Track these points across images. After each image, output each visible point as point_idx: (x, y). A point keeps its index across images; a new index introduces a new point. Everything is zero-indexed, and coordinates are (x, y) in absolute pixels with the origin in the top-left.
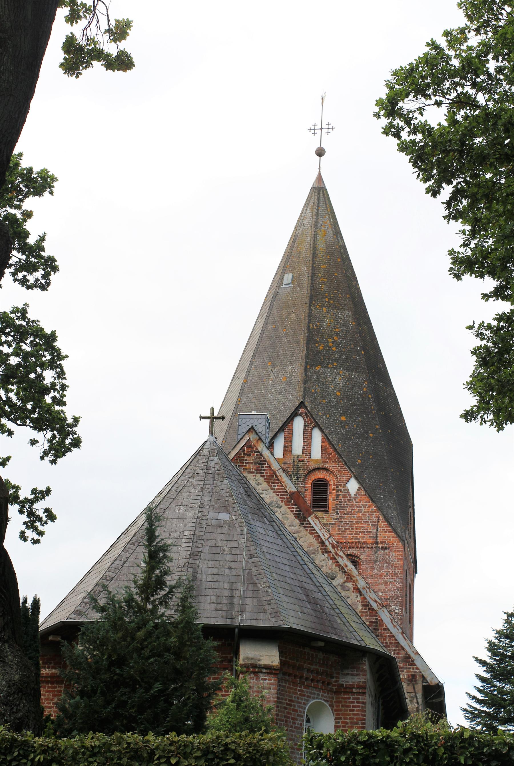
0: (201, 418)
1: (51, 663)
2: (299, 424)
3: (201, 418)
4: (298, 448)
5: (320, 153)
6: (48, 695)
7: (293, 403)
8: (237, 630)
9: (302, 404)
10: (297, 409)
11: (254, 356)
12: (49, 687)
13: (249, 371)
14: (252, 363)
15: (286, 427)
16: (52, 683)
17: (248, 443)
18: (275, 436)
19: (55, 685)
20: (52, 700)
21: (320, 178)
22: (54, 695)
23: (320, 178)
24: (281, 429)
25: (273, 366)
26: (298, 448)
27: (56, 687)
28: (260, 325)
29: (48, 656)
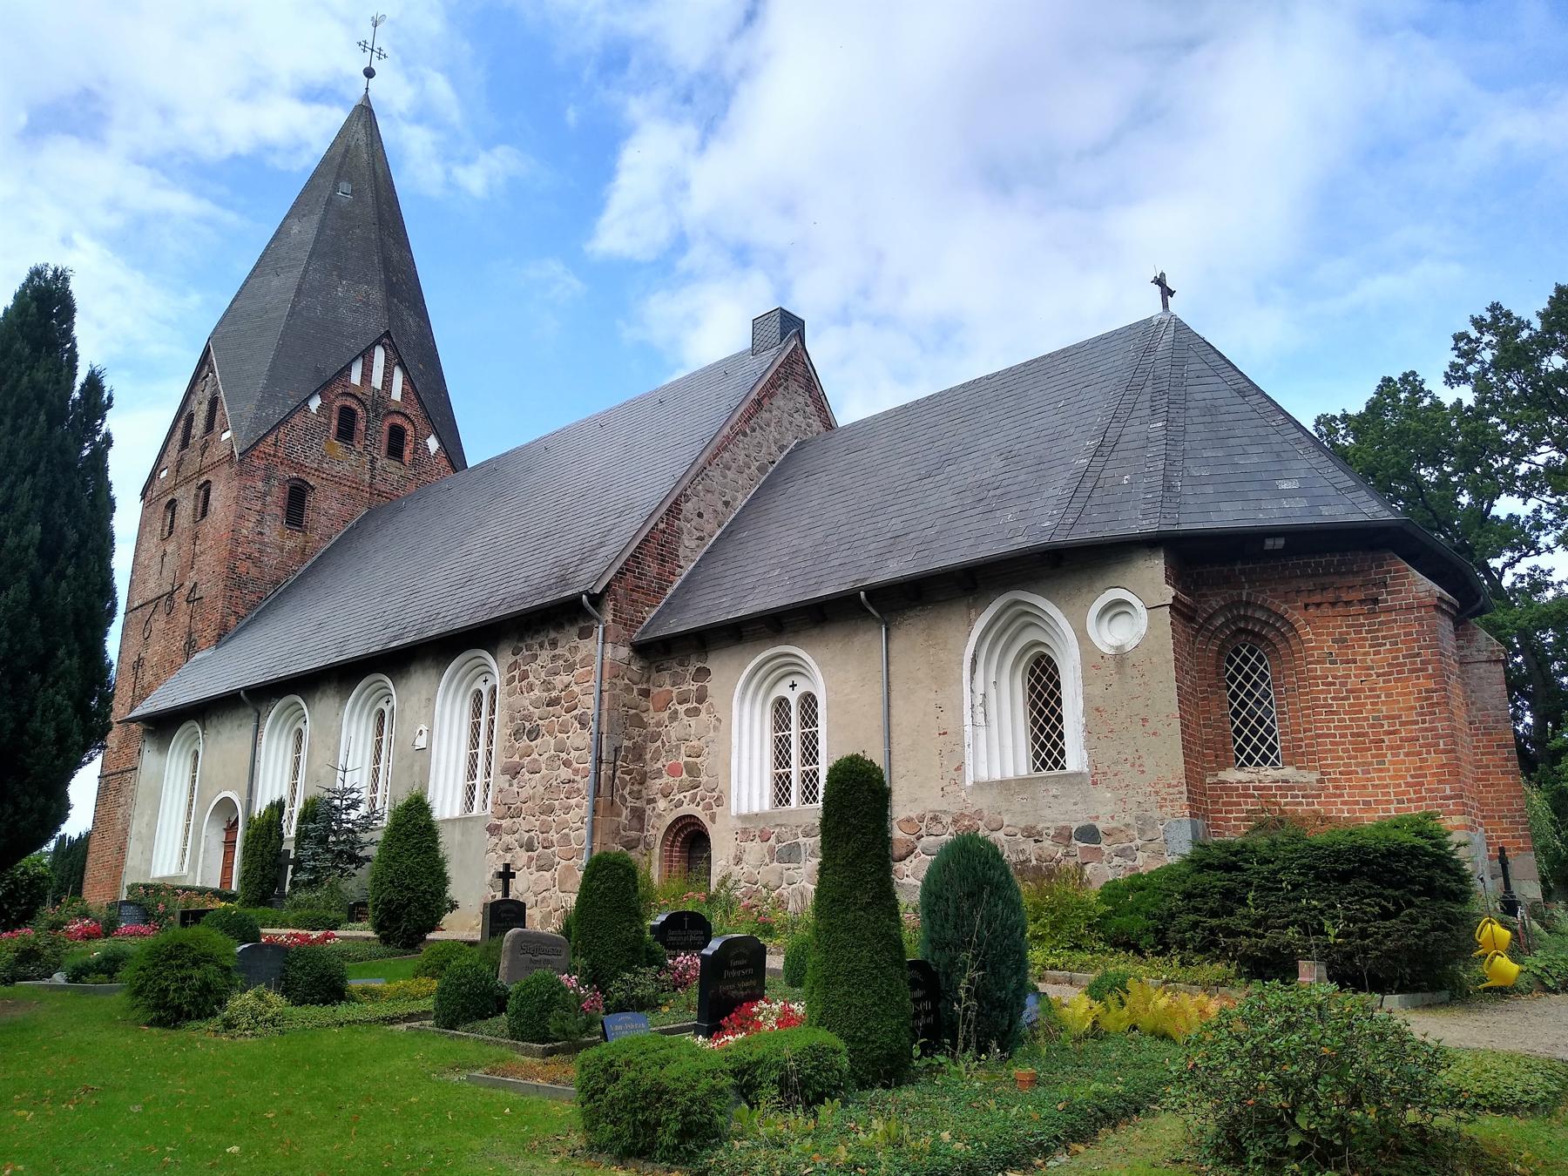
2: (379, 355)
4: (377, 380)
7: (376, 324)
13: (306, 271)
15: (366, 355)
21: (366, 97)
23: (366, 97)
25: (341, 277)
26: (377, 380)
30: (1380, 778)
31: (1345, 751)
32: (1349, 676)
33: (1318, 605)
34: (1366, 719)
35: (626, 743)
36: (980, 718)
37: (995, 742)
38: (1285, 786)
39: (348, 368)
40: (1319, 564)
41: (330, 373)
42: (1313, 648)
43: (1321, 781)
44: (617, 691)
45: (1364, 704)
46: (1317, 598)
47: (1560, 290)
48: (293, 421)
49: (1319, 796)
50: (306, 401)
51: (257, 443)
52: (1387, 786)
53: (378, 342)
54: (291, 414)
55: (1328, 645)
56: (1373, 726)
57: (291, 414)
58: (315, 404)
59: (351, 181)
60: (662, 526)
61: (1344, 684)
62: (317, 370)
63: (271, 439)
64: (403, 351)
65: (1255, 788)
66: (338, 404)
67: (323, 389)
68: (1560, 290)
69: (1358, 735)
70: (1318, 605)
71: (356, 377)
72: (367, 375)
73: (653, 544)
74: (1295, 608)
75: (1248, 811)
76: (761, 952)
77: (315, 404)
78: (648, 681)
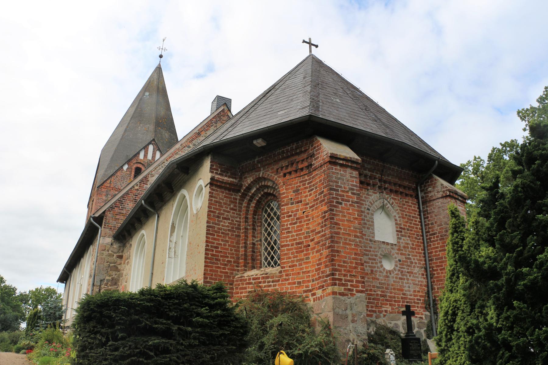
0: (304, 41)
1: (227, 173)
2: (151, 148)
3: (304, 41)
4: (150, 157)
5: (161, 56)
6: (227, 201)
7: (150, 137)
8: (437, 162)
9: (154, 140)
10: (151, 141)
11: (131, 119)
12: (226, 193)
13: (129, 124)
14: (130, 121)
15: (146, 148)
16: (229, 190)
17: (223, 110)
18: (141, 150)
19: (231, 192)
20: (229, 205)
21: (160, 64)
22: (231, 201)
23: (160, 64)
24: (144, 148)
25: (140, 124)
26: (150, 157)
27: (232, 195)
28: (133, 109)
29: (225, 167)
30: (306, 268)
31: (293, 253)
32: (297, 210)
33: (290, 173)
34: (303, 234)
35: (107, 278)
36: (172, 254)
37: (136, 270)
38: (266, 276)
39: (138, 153)
40: (287, 151)
41: (131, 156)
42: (284, 197)
43: (280, 272)
44: (104, 256)
45: (303, 225)
46: (289, 169)
47: (546, 88)
48: (117, 174)
49: (278, 281)
50: (122, 167)
51: (103, 183)
52: (309, 272)
53: (150, 143)
54: (116, 172)
55: (291, 194)
56: (305, 237)
57: (116, 172)
58: (125, 167)
59: (149, 92)
60: (136, 188)
61: (295, 215)
62: (127, 156)
63: (108, 181)
64: (160, 145)
65: (254, 279)
66: (135, 166)
67: (128, 162)
68: (546, 88)
69: (299, 243)
70: (290, 173)
71: (141, 156)
72: (146, 156)
73: (131, 195)
74: (279, 177)
75: (249, 292)
76: (403, 311)
77: (125, 167)
78: (122, 252)
